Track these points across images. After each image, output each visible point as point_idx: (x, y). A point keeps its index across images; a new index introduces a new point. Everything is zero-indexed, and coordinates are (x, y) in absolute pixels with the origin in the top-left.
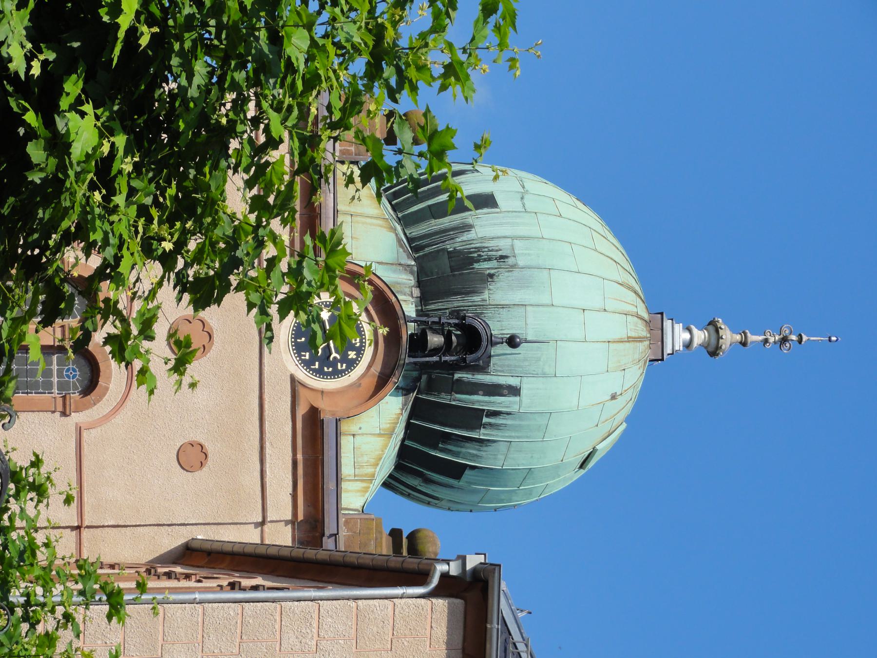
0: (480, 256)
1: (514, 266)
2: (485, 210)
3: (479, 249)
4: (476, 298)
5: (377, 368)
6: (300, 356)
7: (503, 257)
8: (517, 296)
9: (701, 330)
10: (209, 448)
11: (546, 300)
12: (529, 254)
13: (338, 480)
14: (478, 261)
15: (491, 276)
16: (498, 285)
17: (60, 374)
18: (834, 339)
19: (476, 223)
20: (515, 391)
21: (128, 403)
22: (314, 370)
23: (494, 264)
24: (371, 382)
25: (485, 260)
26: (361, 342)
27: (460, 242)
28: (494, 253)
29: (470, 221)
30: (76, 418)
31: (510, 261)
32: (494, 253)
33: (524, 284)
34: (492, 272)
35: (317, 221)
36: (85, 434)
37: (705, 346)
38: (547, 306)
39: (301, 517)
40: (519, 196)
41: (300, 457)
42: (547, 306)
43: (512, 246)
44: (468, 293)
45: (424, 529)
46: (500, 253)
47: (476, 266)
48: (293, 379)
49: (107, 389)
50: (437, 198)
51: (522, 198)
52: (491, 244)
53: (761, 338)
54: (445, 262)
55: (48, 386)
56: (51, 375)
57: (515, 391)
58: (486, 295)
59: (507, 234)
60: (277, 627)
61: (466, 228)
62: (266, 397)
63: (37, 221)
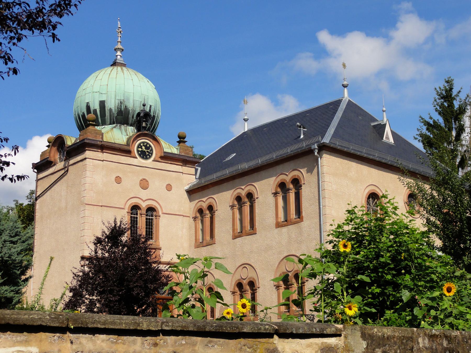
0: (120, 108)
1: (123, 100)
2: (106, 104)
3: (118, 108)
4: (131, 111)
5: (152, 140)
6: (148, 158)
7: (121, 103)
8: (131, 101)
9: (117, 53)
10: (167, 183)
11: (132, 94)
12: (120, 96)
13: (115, 143)
14: (121, 109)
15: (126, 106)
16: (128, 105)
17: (149, 216)
18: (119, 19)
19: (110, 107)
20: (151, 106)
21: (158, 201)
22: (151, 155)
23: (122, 105)
24: (154, 142)
25: (121, 107)
26: (145, 143)
27: (115, 112)
28: (119, 105)
29: (109, 108)
30: (160, 214)
31: (122, 101)
32: (119, 105)
33: (128, 99)
34: (124, 106)
35: (121, 149)
36: (164, 212)
37: (121, 52)
38: (134, 94)
39: (181, 164)
40: (101, 94)
41: (169, 162)
42: (134, 94)
43: (118, 99)
44: (129, 113)
45: (178, 134)
46: (120, 103)
47: (122, 110)
48: (153, 161)
49: (155, 206)
50: (98, 115)
51: (102, 94)
52: (117, 105)
53: (119, 37)
54: (119, 117)
55: (152, 219)
56: (135, 217)
57: (151, 106)
58: (130, 109)
59: (114, 100)
60: (328, 191)
61: (111, 110)
62: (157, 168)
63: (468, 242)
